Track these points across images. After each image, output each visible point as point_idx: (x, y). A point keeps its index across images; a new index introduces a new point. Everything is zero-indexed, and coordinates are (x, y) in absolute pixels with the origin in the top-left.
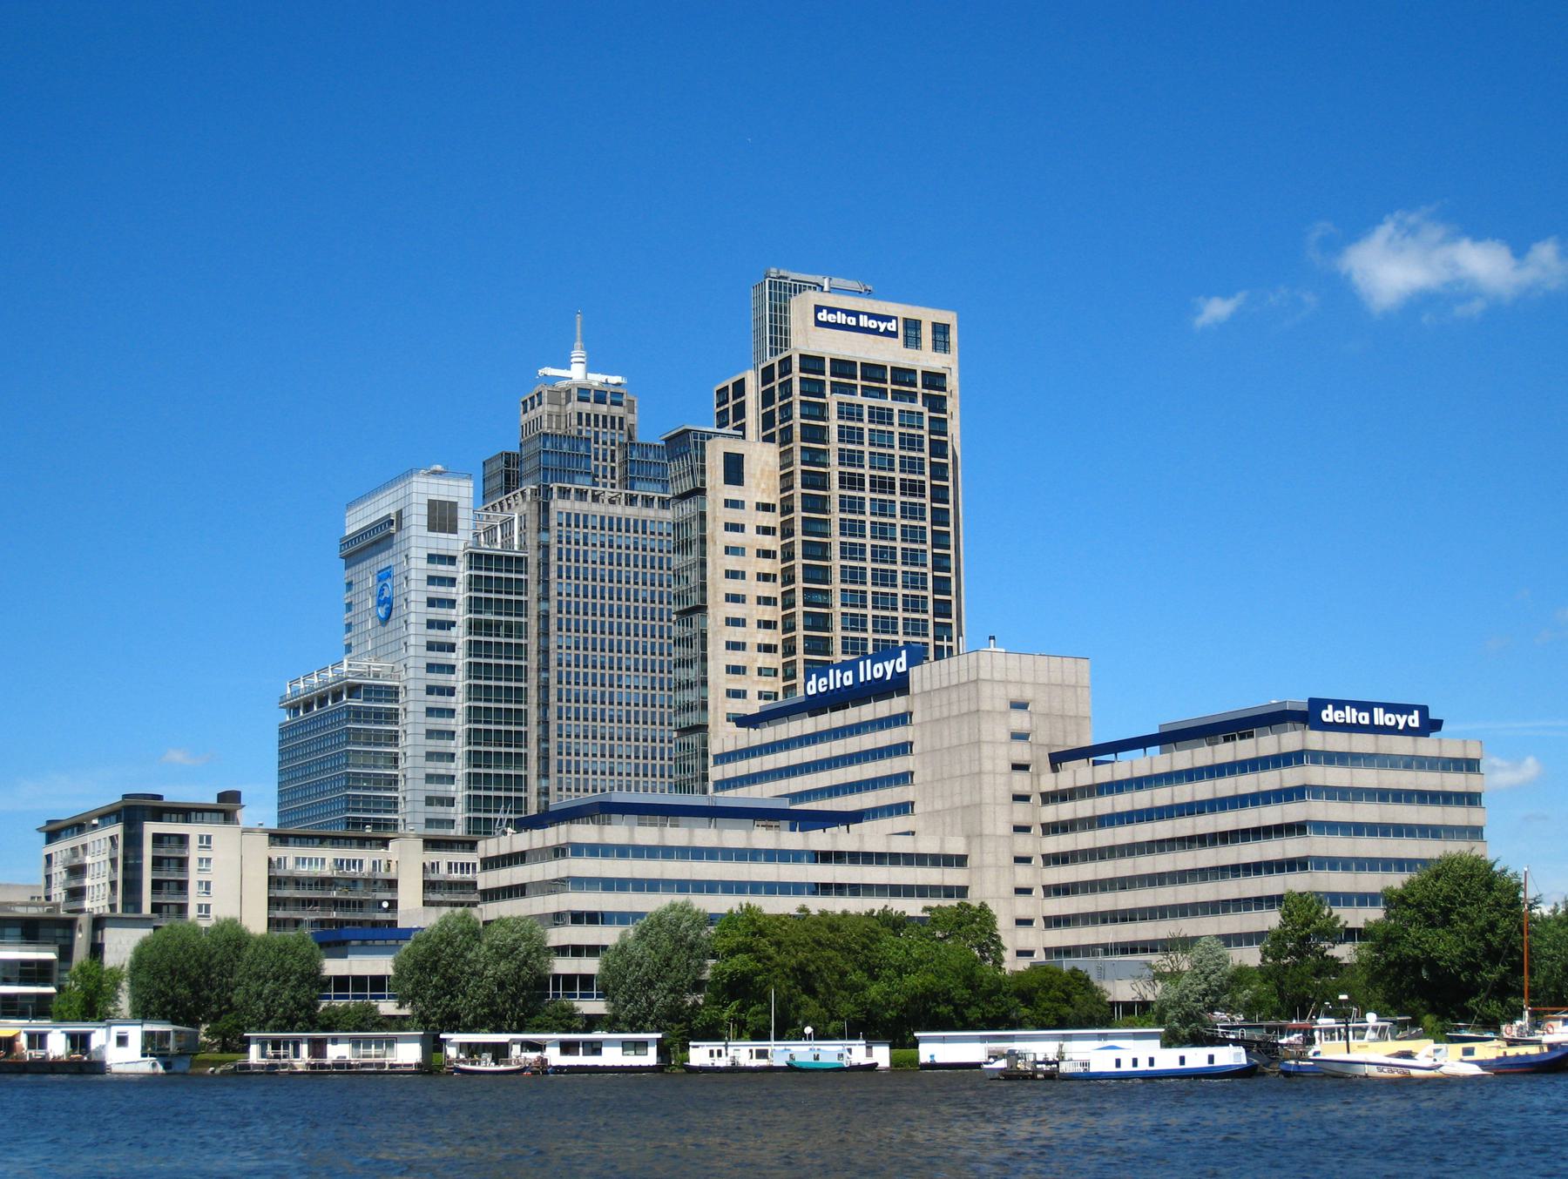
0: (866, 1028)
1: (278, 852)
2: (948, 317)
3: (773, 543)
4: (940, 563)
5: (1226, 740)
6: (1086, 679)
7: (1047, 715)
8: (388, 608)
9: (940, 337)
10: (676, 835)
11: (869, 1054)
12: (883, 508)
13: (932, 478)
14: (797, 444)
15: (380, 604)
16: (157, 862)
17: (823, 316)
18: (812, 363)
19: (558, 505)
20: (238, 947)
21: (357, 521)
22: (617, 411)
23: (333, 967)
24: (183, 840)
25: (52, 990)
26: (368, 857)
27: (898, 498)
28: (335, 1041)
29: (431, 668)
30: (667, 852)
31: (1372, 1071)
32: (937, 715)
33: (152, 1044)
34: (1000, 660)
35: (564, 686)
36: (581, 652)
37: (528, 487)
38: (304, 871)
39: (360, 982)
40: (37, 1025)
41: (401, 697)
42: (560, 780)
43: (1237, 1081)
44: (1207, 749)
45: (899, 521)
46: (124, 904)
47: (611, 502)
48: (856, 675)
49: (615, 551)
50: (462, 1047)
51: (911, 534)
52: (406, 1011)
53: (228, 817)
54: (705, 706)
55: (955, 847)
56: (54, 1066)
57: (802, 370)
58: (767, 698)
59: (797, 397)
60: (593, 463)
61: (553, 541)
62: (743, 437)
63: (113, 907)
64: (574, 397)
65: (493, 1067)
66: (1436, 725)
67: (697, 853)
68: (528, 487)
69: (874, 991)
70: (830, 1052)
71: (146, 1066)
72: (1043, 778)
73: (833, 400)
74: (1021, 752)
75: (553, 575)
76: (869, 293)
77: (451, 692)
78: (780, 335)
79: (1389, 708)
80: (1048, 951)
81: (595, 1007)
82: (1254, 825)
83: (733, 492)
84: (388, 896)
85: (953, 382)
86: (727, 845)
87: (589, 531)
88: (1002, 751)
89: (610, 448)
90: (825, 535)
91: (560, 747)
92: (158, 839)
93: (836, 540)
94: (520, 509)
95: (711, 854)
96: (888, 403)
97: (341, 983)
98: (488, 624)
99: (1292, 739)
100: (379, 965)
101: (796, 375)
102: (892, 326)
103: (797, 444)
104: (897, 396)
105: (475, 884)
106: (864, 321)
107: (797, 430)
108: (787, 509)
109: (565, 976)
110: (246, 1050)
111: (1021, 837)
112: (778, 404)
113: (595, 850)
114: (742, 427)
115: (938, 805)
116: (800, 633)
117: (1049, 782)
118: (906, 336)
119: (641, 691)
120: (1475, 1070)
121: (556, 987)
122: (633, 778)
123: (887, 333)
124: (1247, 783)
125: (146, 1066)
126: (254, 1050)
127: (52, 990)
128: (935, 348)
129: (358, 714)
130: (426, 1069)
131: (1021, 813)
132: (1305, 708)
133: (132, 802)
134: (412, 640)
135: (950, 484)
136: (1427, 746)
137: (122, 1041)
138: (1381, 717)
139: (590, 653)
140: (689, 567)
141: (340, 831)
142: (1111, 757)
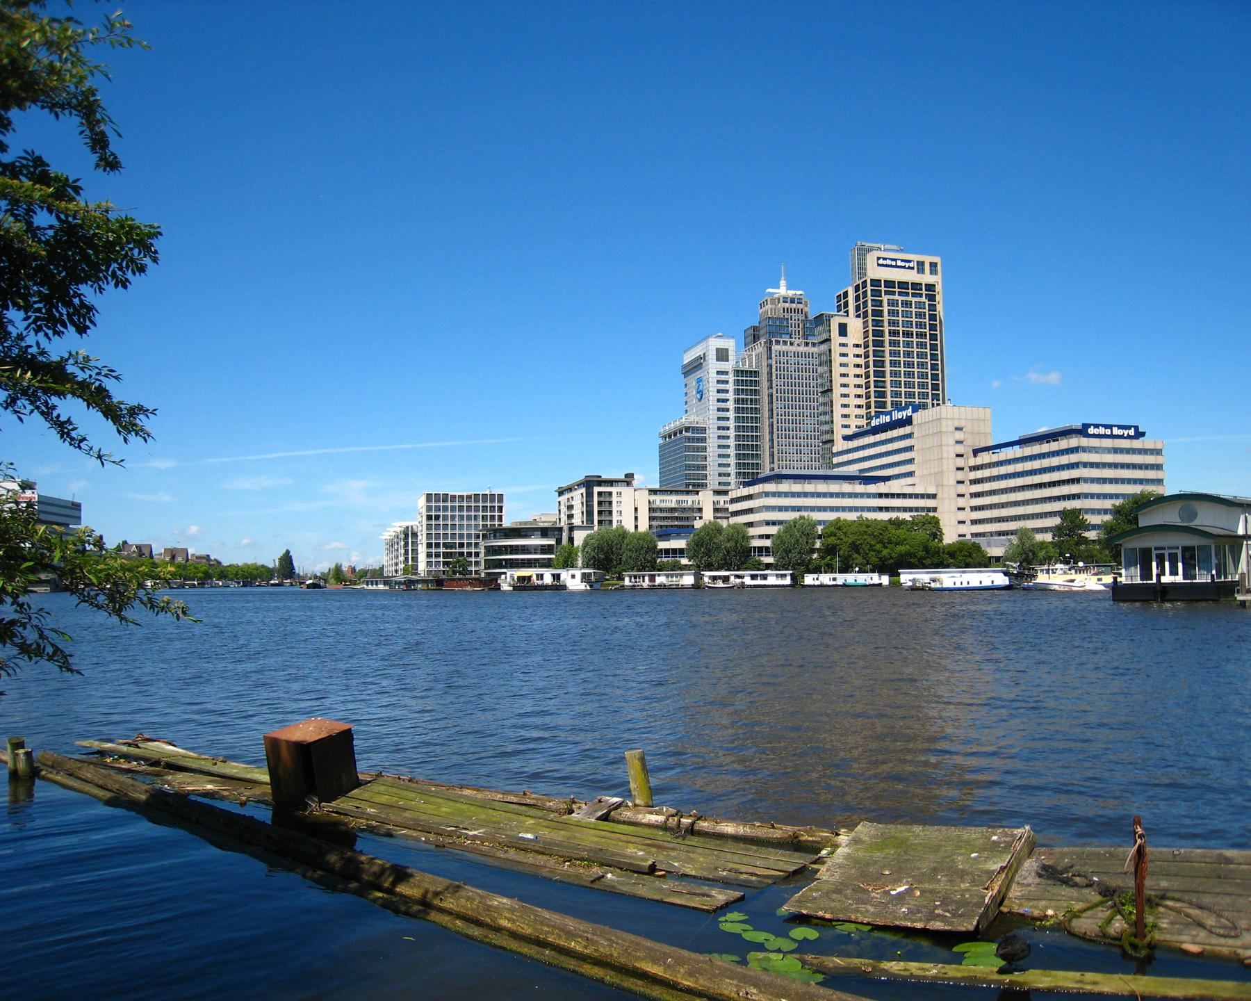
0: (881, 570)
1: (653, 498)
2: (937, 259)
3: (861, 361)
4: (934, 367)
5: (1047, 442)
6: (989, 416)
7: (972, 433)
8: (701, 394)
9: (920, 267)
10: (809, 487)
11: (880, 579)
12: (908, 344)
13: (930, 330)
14: (870, 318)
15: (698, 392)
16: (600, 503)
17: (881, 262)
18: (875, 282)
19: (775, 348)
20: (624, 537)
21: (688, 358)
22: (800, 306)
23: (662, 545)
24: (610, 494)
25: (553, 556)
26: (690, 500)
27: (915, 340)
28: (659, 575)
29: (719, 419)
30: (806, 495)
31: (1057, 588)
32: (924, 434)
33: (585, 578)
34: (950, 409)
35: (780, 425)
36: (787, 410)
37: (763, 341)
38: (663, 505)
39: (674, 551)
40: (540, 571)
41: (707, 431)
42: (779, 464)
43: (1003, 592)
44: (1038, 446)
45: (915, 350)
46: (587, 520)
47: (799, 345)
48: (891, 417)
49: (800, 366)
50: (710, 577)
51: (920, 355)
52: (690, 563)
53: (629, 484)
54: (833, 432)
55: (931, 490)
56: (546, 587)
57: (871, 286)
58: (860, 427)
59: (869, 298)
60: (790, 329)
61: (774, 363)
62: (848, 316)
63: (583, 522)
64: (781, 301)
65: (723, 585)
66: (1143, 434)
67: (819, 495)
68: (763, 341)
69: (885, 552)
70: (863, 579)
71: (583, 586)
72: (970, 460)
73: (885, 298)
74: (960, 449)
75: (774, 377)
76: (902, 250)
77: (728, 429)
78: (862, 269)
79: (1120, 427)
80: (973, 535)
81: (770, 560)
82: (1068, 478)
83: (843, 340)
84: (699, 515)
85: (939, 288)
86: (831, 491)
87: (789, 358)
88: (951, 449)
89: (797, 322)
90: (883, 357)
91: (778, 450)
92: (600, 494)
93: (888, 359)
94: (760, 348)
95: (825, 495)
96: (910, 298)
97: (667, 551)
98: (743, 399)
99: (1074, 442)
100: (680, 544)
101: (869, 288)
102: (911, 265)
103: (870, 318)
104: (914, 295)
105: (728, 509)
106: (899, 263)
107: (870, 312)
108: (866, 346)
109: (759, 547)
110: (623, 580)
111: (960, 486)
112: (862, 301)
113: (774, 494)
114: (847, 312)
115: (925, 473)
116: (873, 399)
117: (973, 462)
118: (918, 269)
119: (813, 426)
120: (1102, 588)
121: (755, 552)
122: (810, 463)
123: (910, 268)
124: (1055, 461)
125: (583, 586)
126: (627, 579)
127: (553, 556)
128: (931, 273)
129: (689, 439)
130: (697, 586)
131: (960, 476)
132: (1081, 428)
133: (589, 479)
134: (711, 408)
135: (938, 332)
136: (1137, 444)
137: (573, 576)
138: (1116, 431)
139: (790, 410)
140: (825, 373)
141: (683, 488)
142: (998, 450)
